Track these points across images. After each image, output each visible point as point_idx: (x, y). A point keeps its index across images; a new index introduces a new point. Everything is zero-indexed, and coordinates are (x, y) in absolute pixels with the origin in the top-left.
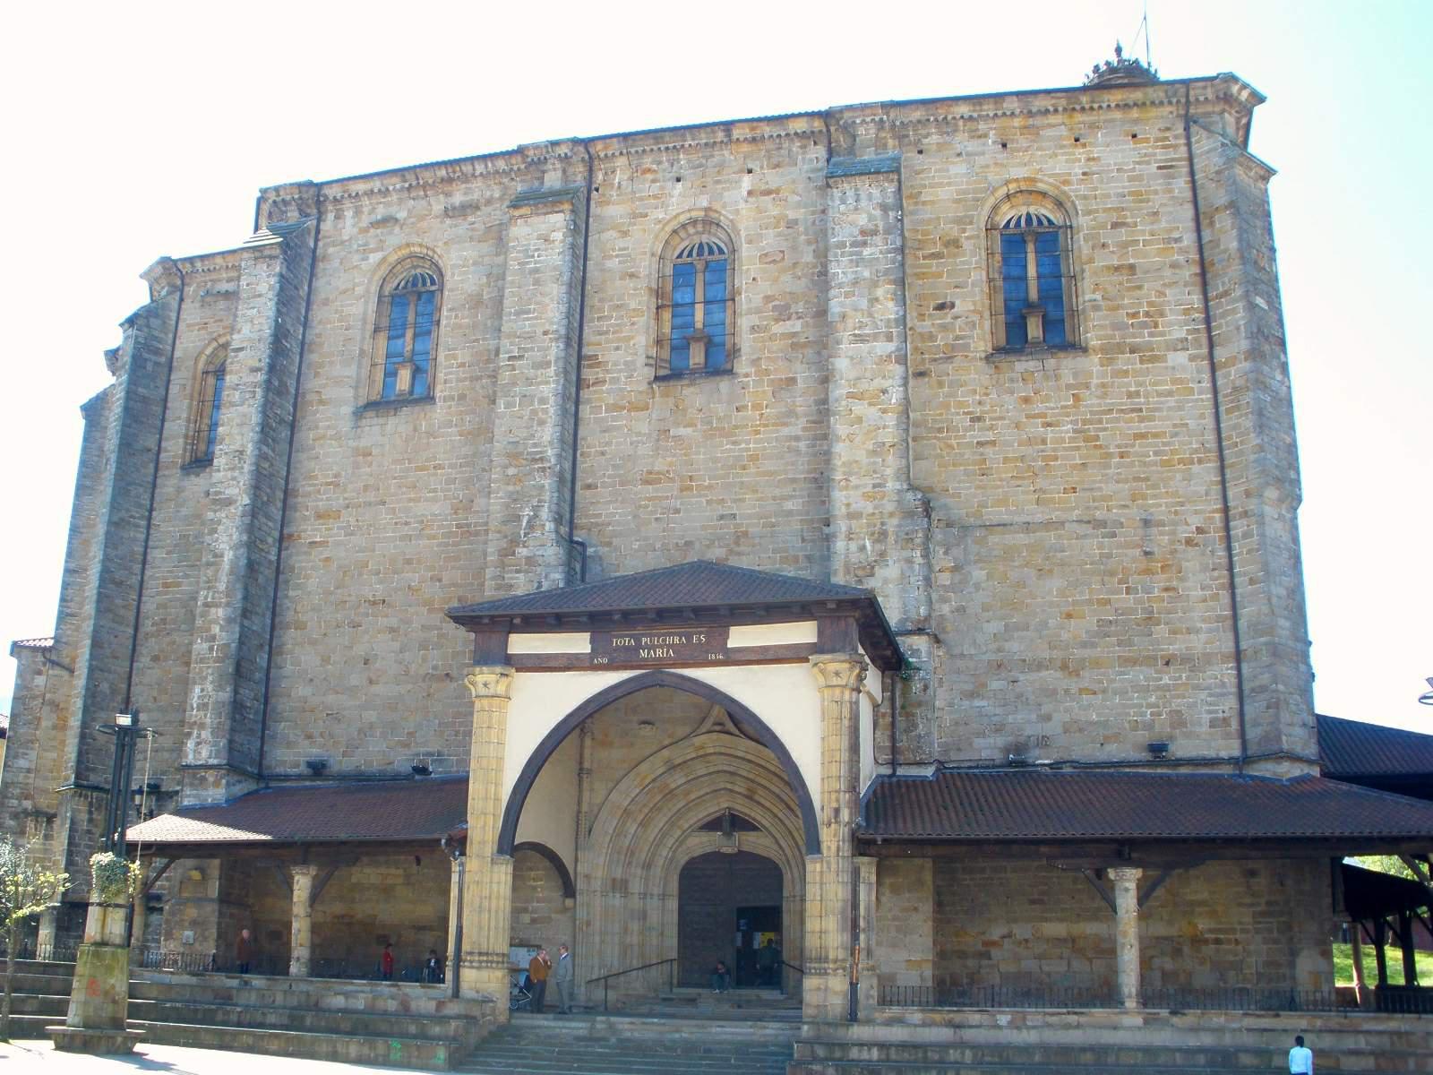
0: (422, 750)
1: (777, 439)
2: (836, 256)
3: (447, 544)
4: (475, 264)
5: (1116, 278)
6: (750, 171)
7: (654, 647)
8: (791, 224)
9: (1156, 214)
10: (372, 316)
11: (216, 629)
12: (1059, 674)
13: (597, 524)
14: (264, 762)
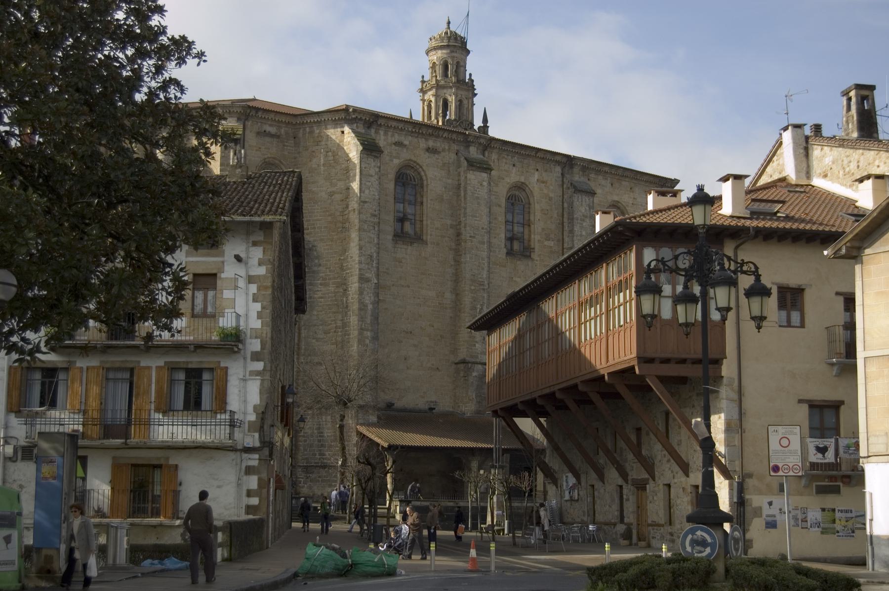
8: (550, 199)
11: (367, 341)
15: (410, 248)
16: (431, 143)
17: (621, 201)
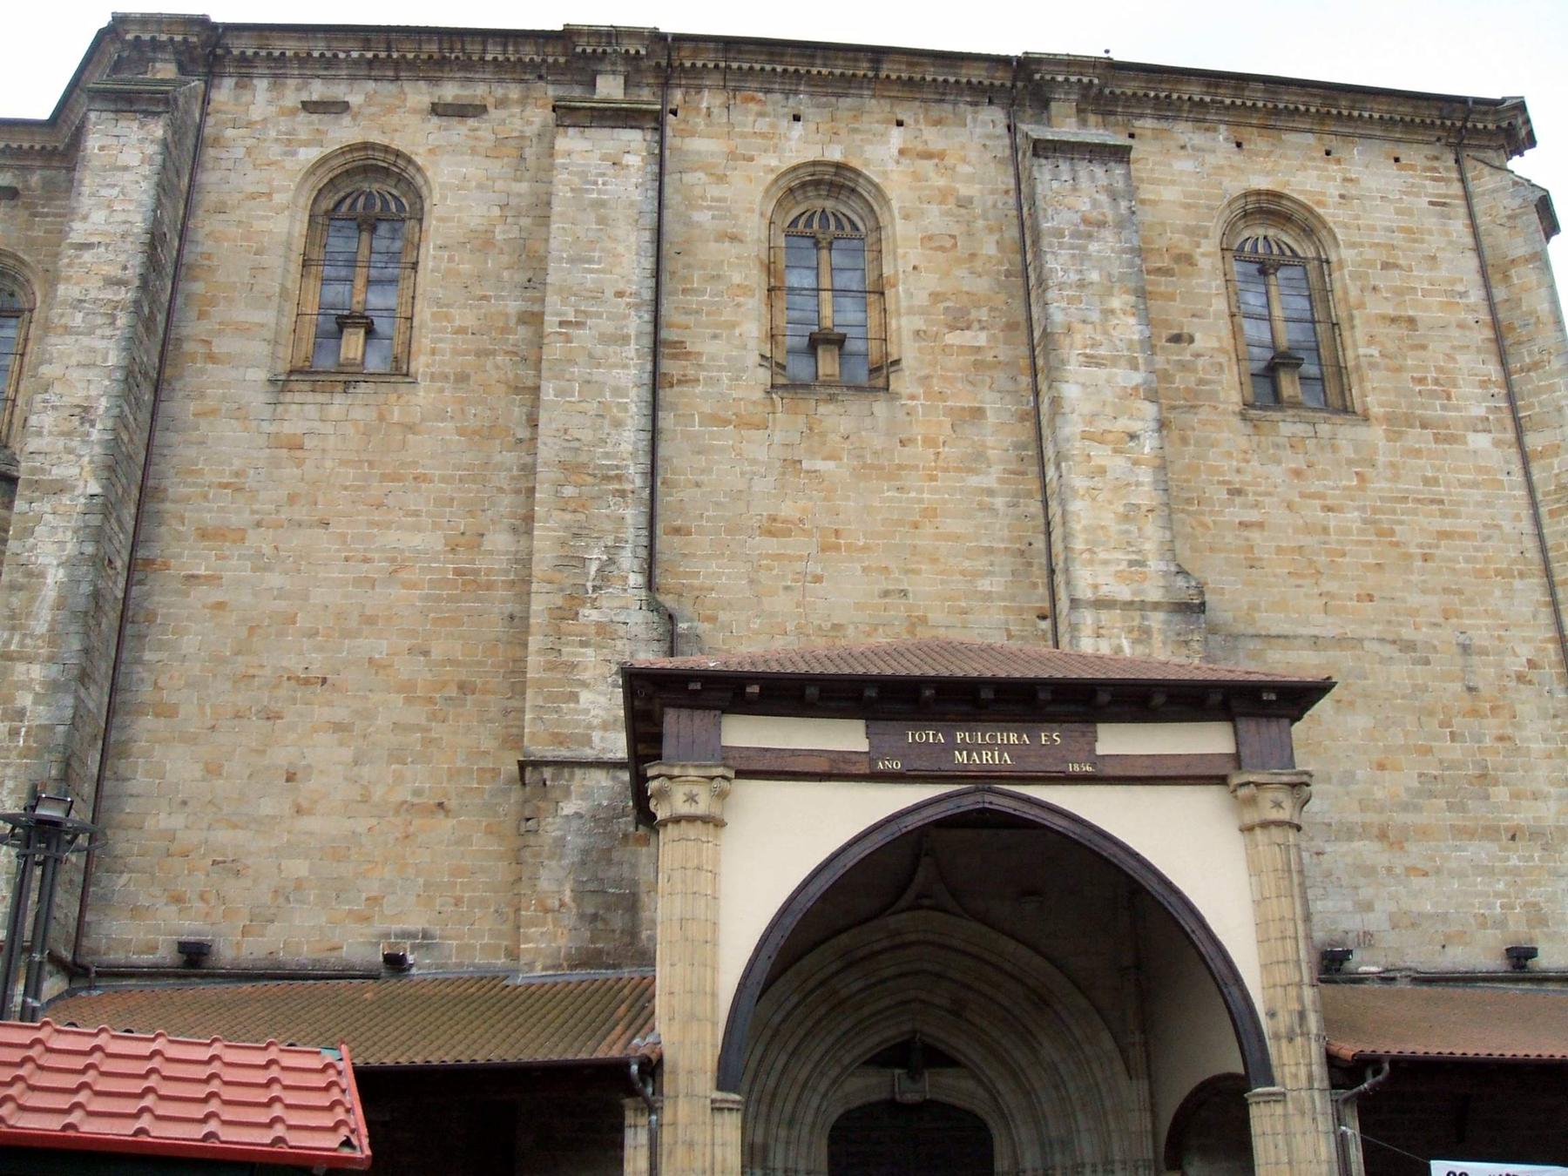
0: (396, 927)
1: (961, 490)
2: (1051, 245)
3: (438, 599)
4: (480, 186)
5: (1394, 330)
6: (900, 124)
7: (979, 748)
8: (964, 203)
9: (1434, 258)
10: (299, 244)
12: (1376, 846)
13: (692, 588)
14: (85, 942)
15: (339, 398)
16: (450, 92)
17: (1286, 191)
